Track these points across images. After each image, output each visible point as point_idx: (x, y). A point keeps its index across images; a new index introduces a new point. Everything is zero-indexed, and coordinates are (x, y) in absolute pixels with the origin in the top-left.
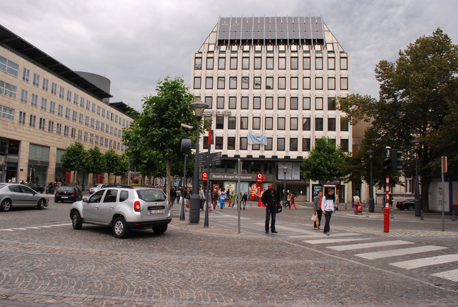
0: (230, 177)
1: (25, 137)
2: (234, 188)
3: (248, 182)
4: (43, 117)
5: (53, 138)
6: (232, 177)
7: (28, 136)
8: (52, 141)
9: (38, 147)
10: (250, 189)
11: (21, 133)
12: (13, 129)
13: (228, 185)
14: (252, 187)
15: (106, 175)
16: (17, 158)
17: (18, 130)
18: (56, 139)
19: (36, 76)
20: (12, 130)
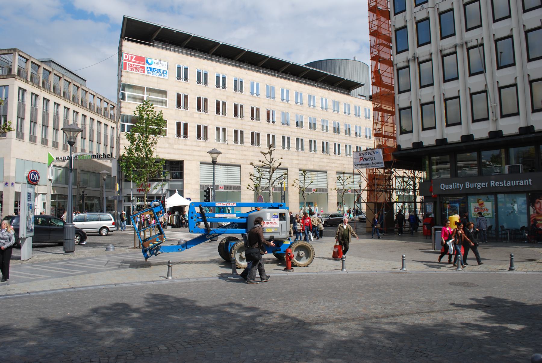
0: (479, 185)
1: (189, 155)
2: (490, 211)
3: (526, 192)
4: (300, 137)
5: (245, 153)
6: (483, 184)
7: (195, 153)
8: (244, 157)
9: (317, 168)
10: (531, 212)
11: (182, 150)
12: (167, 145)
13: (477, 205)
14: (538, 206)
15: (530, 184)
16: (180, 183)
17: (176, 146)
18: (252, 154)
19: (312, 98)
20: (165, 148)
